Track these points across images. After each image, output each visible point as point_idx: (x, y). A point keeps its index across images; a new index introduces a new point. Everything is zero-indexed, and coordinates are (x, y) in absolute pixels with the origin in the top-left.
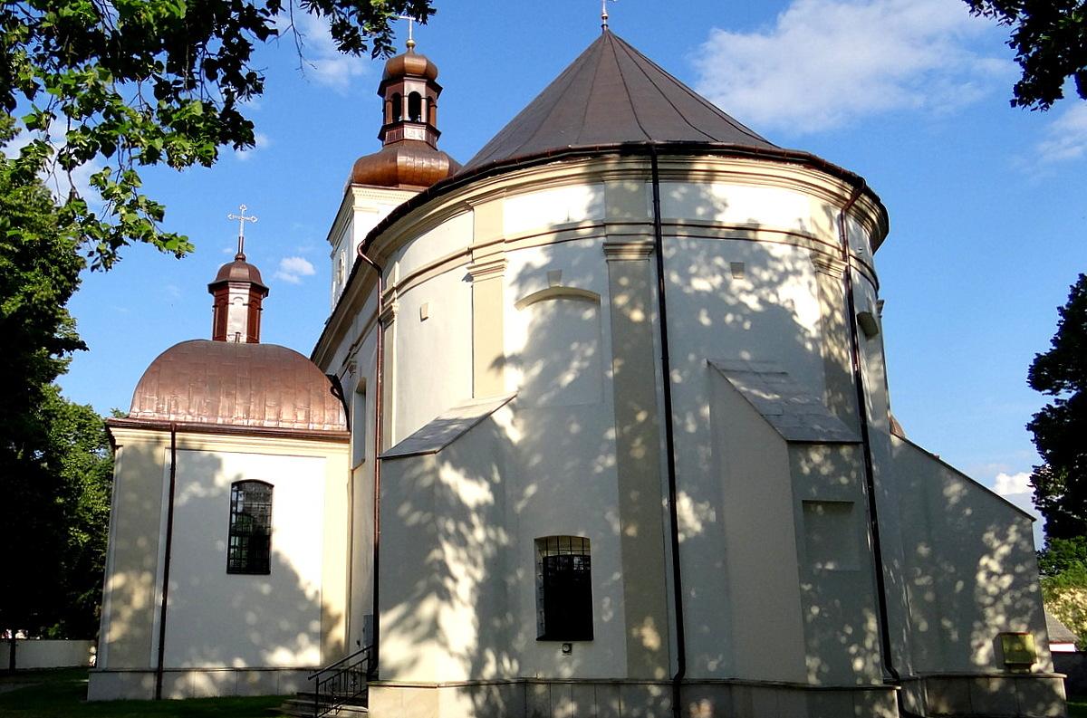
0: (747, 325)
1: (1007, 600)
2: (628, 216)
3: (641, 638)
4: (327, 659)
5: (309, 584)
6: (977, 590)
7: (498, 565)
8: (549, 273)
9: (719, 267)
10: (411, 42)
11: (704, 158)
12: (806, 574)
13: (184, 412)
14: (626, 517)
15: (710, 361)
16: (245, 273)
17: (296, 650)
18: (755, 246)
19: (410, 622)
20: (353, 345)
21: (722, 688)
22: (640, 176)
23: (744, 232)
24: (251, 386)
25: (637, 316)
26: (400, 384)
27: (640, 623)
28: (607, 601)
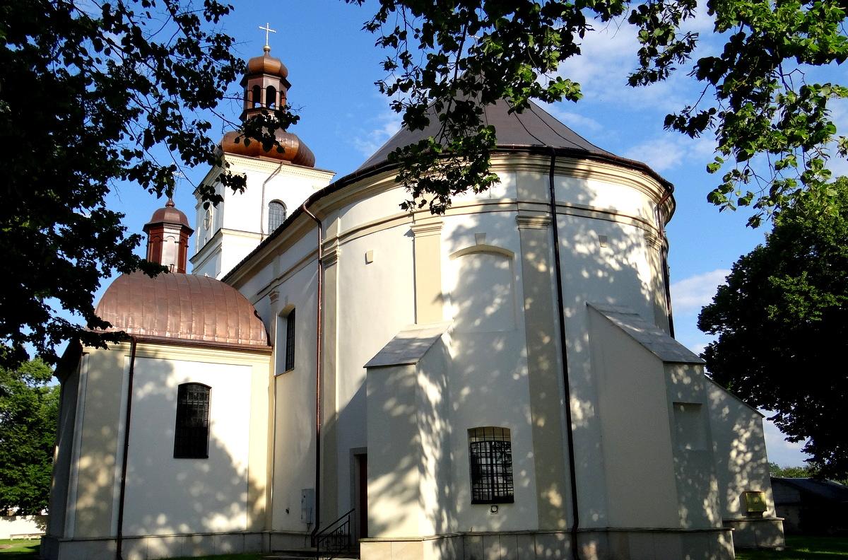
0: (612, 280)
1: (748, 468)
2: (534, 197)
3: (548, 498)
4: (254, 523)
5: (240, 463)
6: (731, 462)
7: (447, 444)
8: (476, 234)
9: (592, 237)
10: (268, 47)
11: (584, 161)
12: (677, 452)
13: (139, 327)
14: (537, 411)
15: (588, 303)
16: (176, 217)
17: (230, 516)
18: (614, 225)
19: (398, 488)
20: (277, 279)
21: (604, 533)
22: (542, 169)
23: (607, 215)
24: (143, 303)
25: (542, 268)
26: (343, 311)
27: (548, 487)
28: (523, 473)
